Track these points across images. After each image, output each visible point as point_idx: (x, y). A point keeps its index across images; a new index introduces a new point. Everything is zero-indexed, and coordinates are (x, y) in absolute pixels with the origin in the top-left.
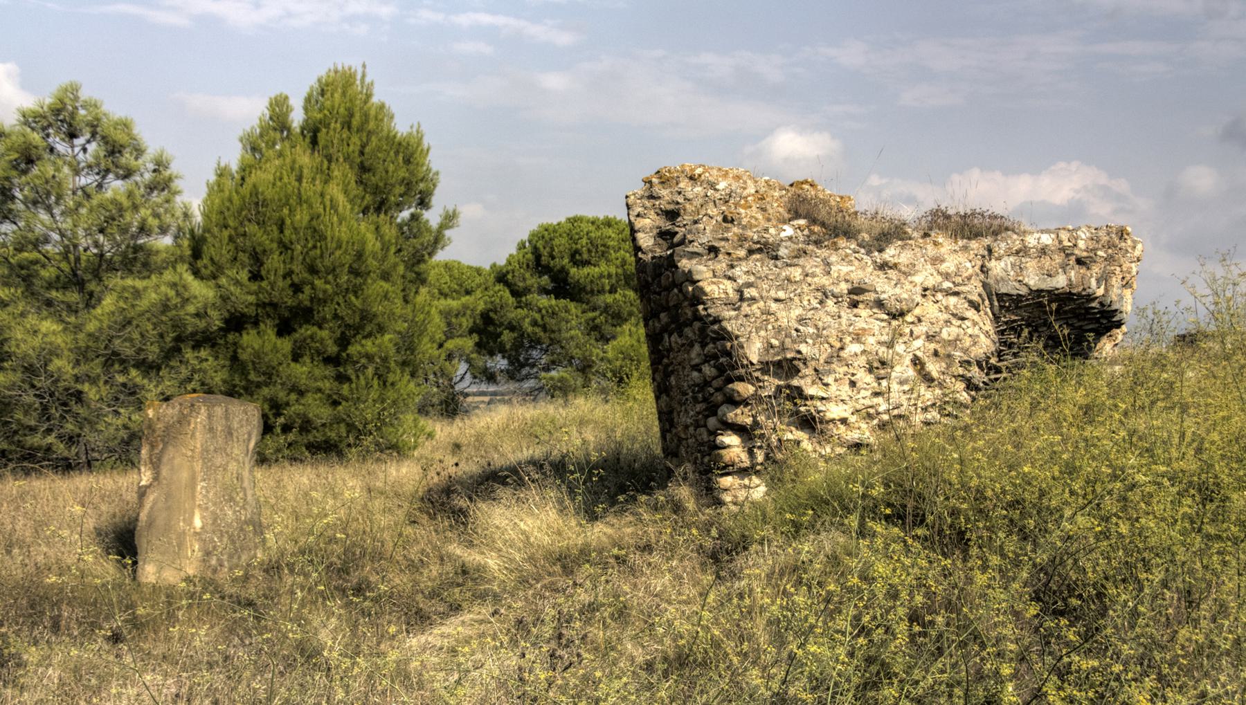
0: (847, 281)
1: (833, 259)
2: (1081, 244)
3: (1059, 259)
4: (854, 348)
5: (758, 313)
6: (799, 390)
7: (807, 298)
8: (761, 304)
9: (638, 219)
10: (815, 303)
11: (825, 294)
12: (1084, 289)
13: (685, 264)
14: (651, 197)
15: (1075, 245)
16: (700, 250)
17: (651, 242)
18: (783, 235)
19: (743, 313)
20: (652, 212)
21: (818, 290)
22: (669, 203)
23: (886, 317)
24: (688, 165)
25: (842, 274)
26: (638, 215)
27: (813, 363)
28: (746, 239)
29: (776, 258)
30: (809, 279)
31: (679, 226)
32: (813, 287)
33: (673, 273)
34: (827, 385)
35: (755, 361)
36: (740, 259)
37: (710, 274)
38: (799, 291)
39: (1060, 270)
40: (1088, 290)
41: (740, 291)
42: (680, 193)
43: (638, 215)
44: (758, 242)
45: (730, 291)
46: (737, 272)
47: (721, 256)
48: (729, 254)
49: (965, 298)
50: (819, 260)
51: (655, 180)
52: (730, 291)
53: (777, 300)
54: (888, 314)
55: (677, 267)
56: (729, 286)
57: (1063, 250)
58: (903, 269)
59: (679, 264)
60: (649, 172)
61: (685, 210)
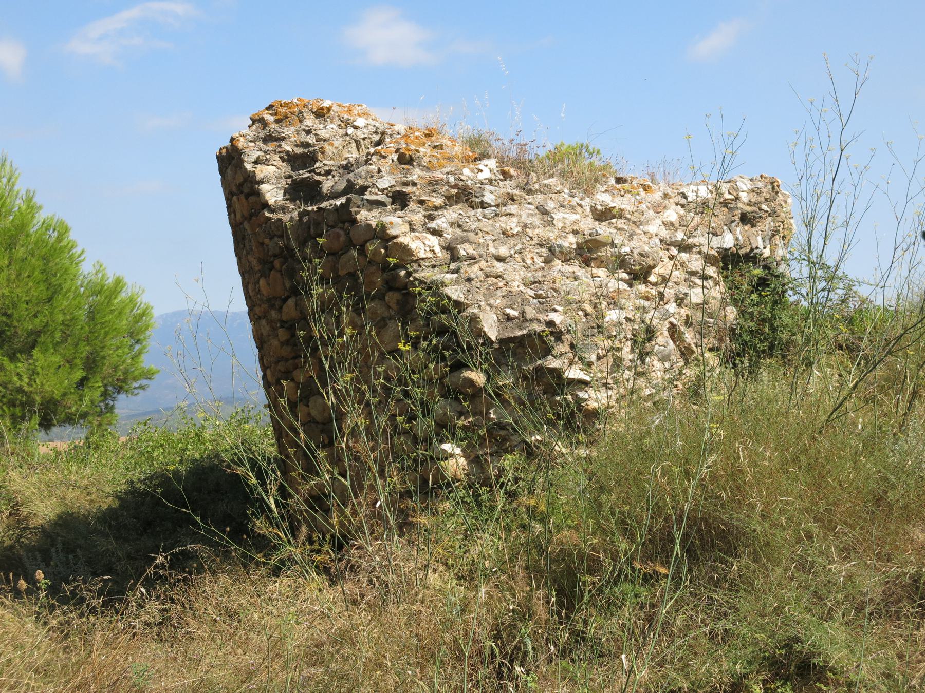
0: (575, 232)
1: (550, 205)
2: (744, 197)
3: (722, 213)
4: (612, 315)
5: (481, 275)
6: (557, 373)
7: (529, 256)
8: (483, 264)
9: (259, 167)
10: (539, 262)
11: (551, 250)
12: (752, 250)
13: (364, 216)
14: (267, 140)
15: (737, 198)
16: (382, 197)
17: (280, 197)
18: (481, 176)
19: (464, 276)
20: (277, 157)
21: (541, 245)
22: (297, 146)
23: (625, 276)
24: (309, 97)
25: (568, 224)
26: (256, 162)
27: (568, 336)
28: (437, 182)
29: (483, 205)
30: (529, 232)
31: (319, 174)
32: (535, 241)
33: (348, 233)
34: (590, 365)
35: (493, 339)
36: (437, 208)
37: (406, 228)
38: (519, 247)
39: (725, 228)
40: (755, 251)
41: (450, 249)
42: (308, 132)
43: (256, 162)
44: (455, 186)
45: (437, 249)
46: (440, 223)
47: (412, 205)
48: (422, 202)
49: (700, 253)
50: (533, 207)
51: (270, 118)
52: (437, 249)
53: (500, 259)
54: (629, 273)
55: (354, 221)
56: (434, 241)
57: (725, 204)
58: (629, 216)
59: (359, 217)
60: (258, 108)
61: (323, 153)
